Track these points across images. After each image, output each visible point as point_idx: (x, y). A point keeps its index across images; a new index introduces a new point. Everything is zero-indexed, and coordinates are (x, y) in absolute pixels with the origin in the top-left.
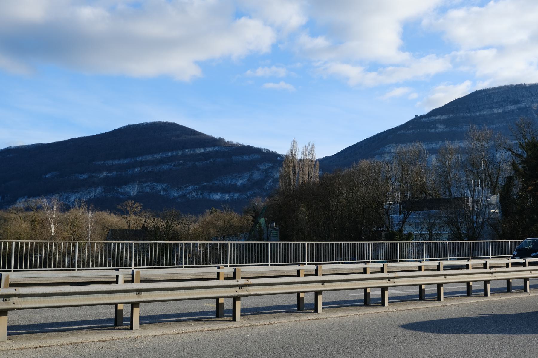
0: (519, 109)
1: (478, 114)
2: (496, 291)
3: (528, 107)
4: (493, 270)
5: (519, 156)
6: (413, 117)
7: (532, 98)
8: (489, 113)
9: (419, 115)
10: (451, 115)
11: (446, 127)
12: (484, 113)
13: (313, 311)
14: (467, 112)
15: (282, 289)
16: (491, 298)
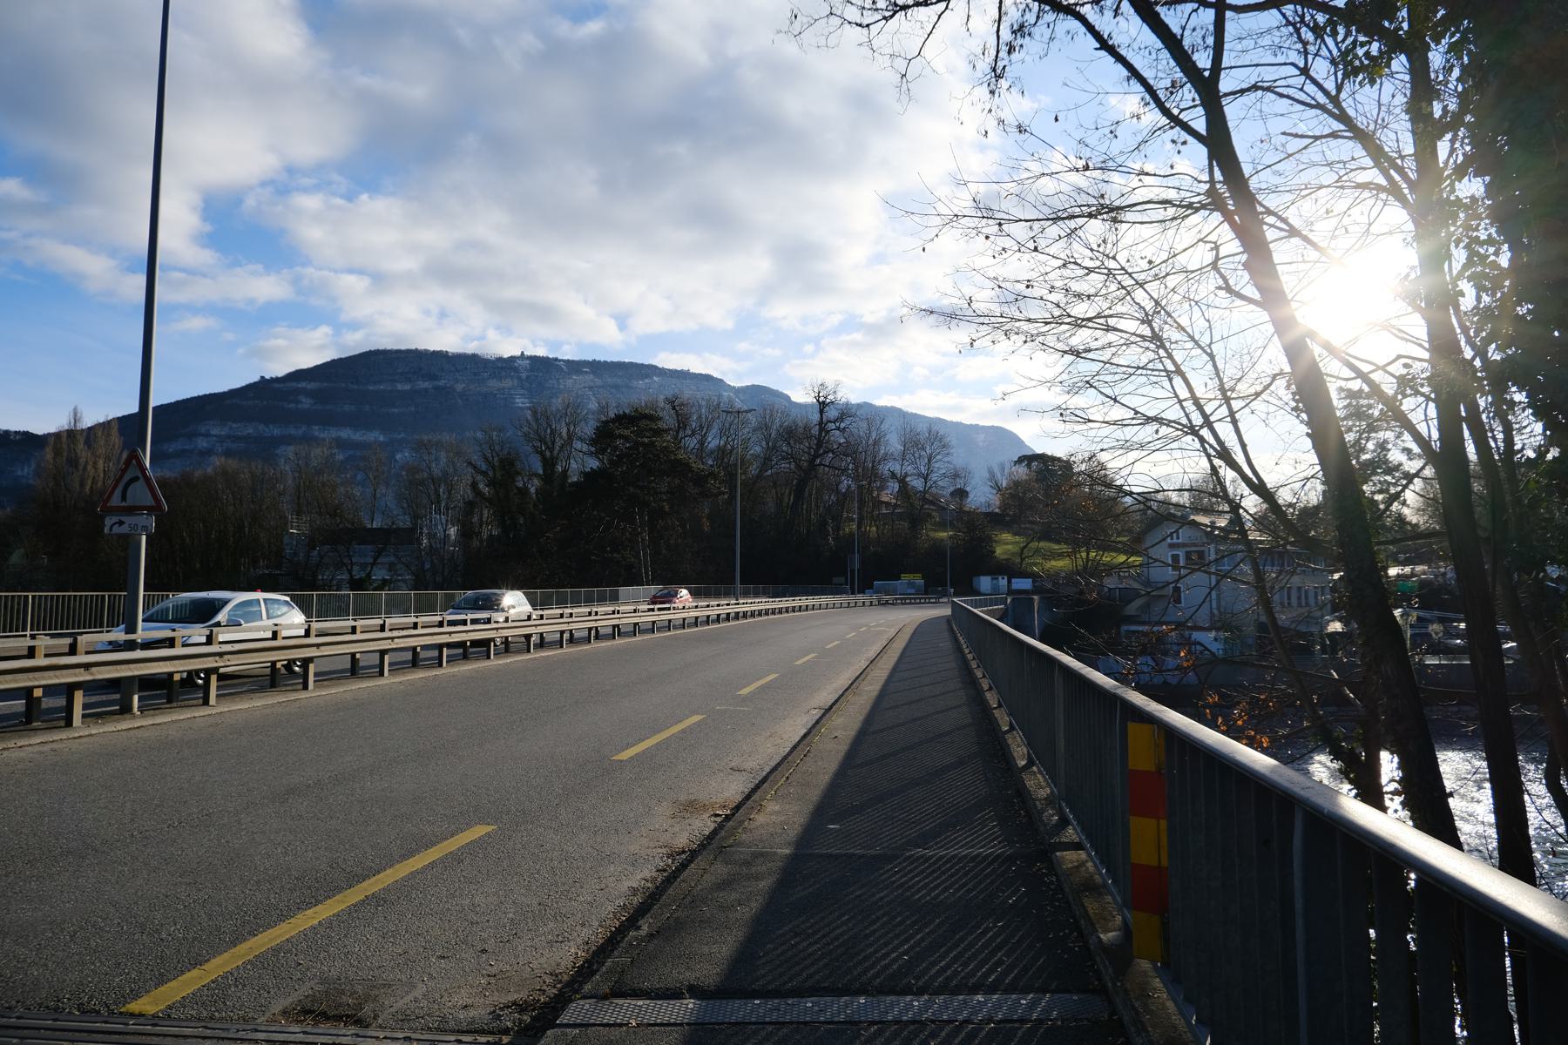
0: (436, 388)
1: (371, 388)
2: (397, 667)
3: (449, 388)
4: (395, 633)
5: (484, 473)
6: (256, 379)
7: (457, 373)
8: (389, 388)
9: (267, 377)
10: (325, 384)
11: (315, 404)
12: (381, 387)
13: (62, 723)
14: (352, 383)
15: (332, 650)
16: (388, 680)
